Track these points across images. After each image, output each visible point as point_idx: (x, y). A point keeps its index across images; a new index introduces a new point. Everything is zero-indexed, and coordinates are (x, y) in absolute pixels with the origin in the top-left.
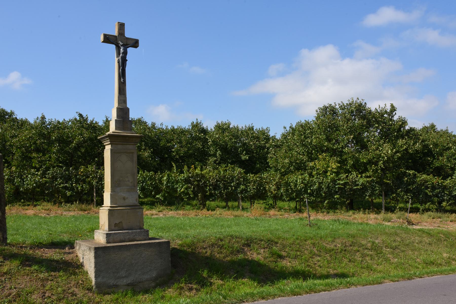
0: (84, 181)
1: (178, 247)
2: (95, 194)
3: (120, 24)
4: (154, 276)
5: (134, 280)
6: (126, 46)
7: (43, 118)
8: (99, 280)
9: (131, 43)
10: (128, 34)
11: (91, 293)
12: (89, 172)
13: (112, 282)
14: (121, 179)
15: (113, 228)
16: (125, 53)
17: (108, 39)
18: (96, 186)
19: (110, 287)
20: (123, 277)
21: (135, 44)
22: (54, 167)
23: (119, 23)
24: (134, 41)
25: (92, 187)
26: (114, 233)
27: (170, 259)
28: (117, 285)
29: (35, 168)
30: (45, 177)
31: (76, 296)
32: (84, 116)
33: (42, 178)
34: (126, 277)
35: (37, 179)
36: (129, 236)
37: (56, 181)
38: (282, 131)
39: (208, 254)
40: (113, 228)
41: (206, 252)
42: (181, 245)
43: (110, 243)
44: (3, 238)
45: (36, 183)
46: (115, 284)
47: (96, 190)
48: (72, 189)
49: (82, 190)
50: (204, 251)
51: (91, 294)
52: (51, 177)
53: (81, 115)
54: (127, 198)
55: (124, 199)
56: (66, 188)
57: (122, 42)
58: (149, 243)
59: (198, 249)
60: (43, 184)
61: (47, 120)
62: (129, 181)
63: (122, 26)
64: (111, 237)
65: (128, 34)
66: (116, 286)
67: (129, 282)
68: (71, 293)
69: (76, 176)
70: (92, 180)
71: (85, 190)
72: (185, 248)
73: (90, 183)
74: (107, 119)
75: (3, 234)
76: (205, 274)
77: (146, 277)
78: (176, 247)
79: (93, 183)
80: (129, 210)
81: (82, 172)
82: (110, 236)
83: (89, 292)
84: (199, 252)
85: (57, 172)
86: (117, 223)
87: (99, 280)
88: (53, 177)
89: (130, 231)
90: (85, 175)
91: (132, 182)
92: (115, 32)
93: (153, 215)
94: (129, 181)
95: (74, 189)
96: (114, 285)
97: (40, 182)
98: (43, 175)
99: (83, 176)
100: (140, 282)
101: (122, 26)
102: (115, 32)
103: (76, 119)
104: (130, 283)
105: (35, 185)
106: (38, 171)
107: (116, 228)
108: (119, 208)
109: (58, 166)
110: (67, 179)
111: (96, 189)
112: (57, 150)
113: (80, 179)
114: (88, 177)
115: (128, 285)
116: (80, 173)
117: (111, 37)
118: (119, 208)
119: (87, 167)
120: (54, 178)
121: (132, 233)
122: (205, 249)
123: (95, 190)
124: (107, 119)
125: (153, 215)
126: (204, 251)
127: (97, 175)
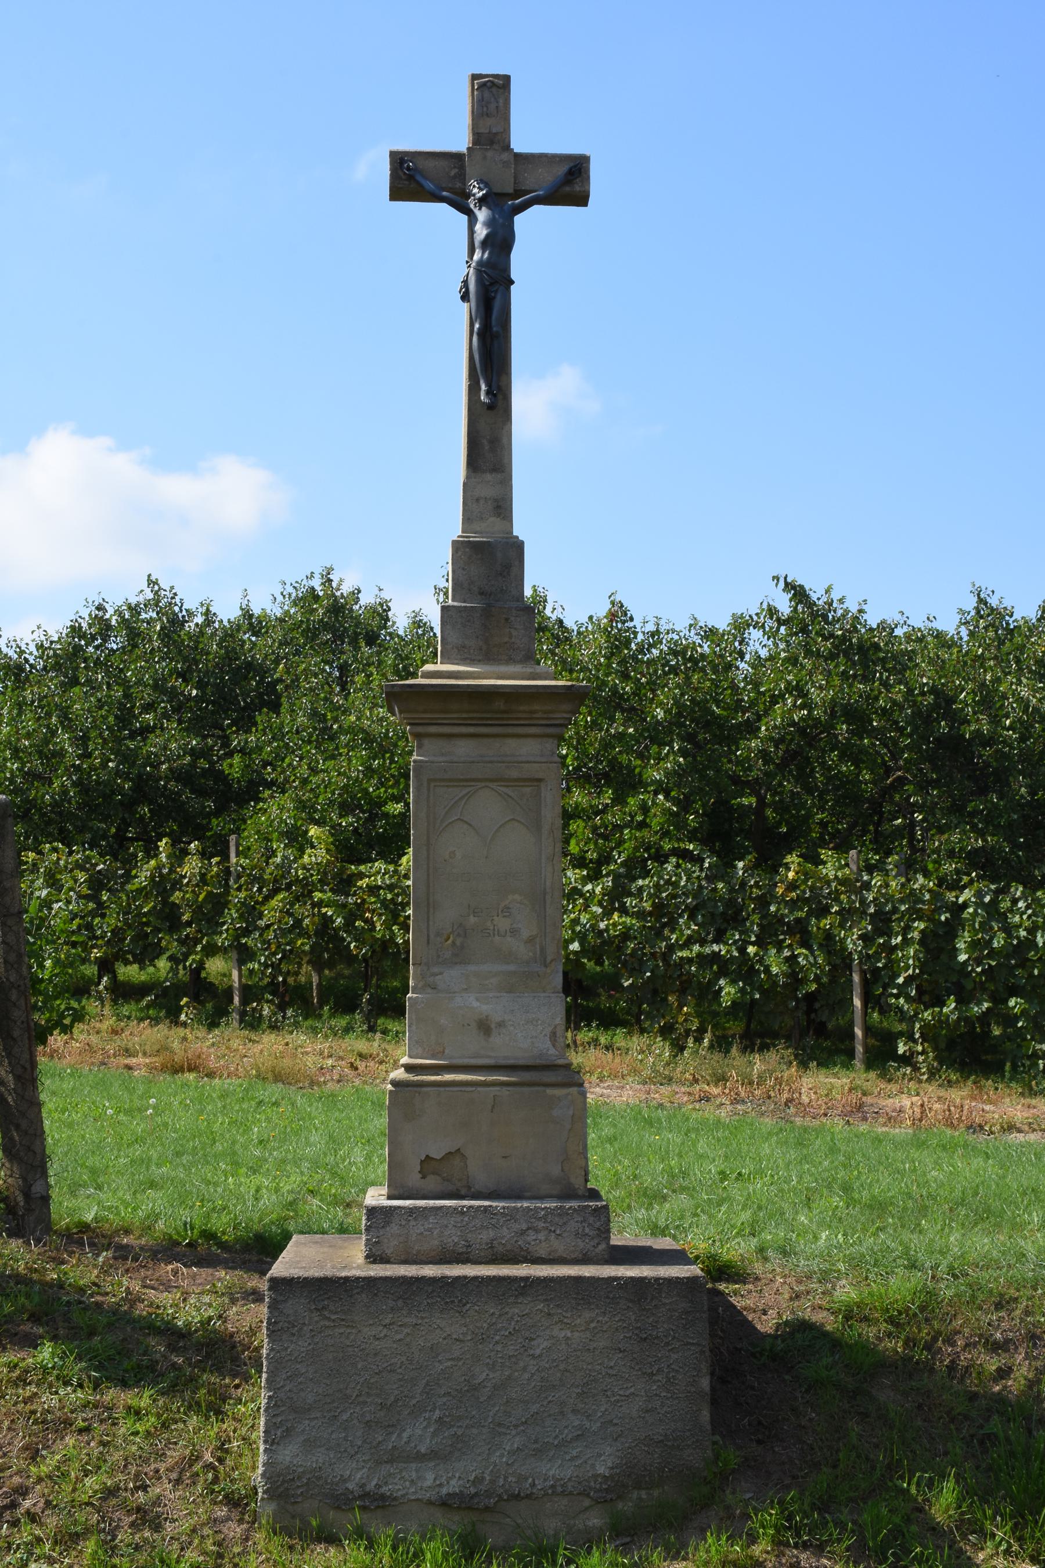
0: (801, 932)
1: (830, 1323)
2: (857, 1002)
3: (482, 86)
4: (601, 1470)
5: (478, 1480)
6: (506, 204)
7: (618, 613)
8: (288, 1454)
9: (545, 179)
10: (530, 134)
11: (241, 1521)
12: (828, 883)
13: (356, 1475)
14: (472, 919)
15: (414, 1179)
16: (500, 242)
17: (413, 178)
18: (866, 958)
19: (342, 1501)
20: (420, 1458)
21: (568, 182)
22: (661, 858)
23: (474, 77)
24: (562, 170)
25: (840, 961)
26: (411, 1211)
27: (705, 1383)
28: (383, 1497)
29: (580, 862)
30: (624, 911)
31: (157, 1528)
32: (817, 594)
33: (607, 914)
34: (433, 1455)
35: (584, 918)
36: (492, 1233)
37: (673, 931)
38: (891, 616)
39: (1015, 1384)
40: (414, 1179)
41: (1003, 1373)
42: (849, 1314)
43: (384, 1260)
44: (27, 1195)
45: (582, 938)
46: (371, 1486)
47: (866, 984)
48: (744, 970)
49: (795, 975)
50: (992, 1364)
51: (234, 1530)
52: (647, 906)
53: (799, 593)
54: (501, 1024)
55: (485, 1027)
56: (722, 966)
57: (491, 180)
58: (579, 1279)
59: (950, 1341)
60: (609, 942)
61: (637, 623)
62: (514, 932)
63: (491, 94)
64: (394, 1228)
65: (530, 134)
66: (378, 1503)
67: (454, 1486)
68: (139, 1509)
69: (763, 903)
70: (842, 926)
71: (804, 981)
72: (870, 1333)
73: (829, 942)
74: (981, 601)
75: (24, 1179)
76: (944, 1503)
77: (554, 1470)
78: (818, 1317)
79: (843, 941)
80: (505, 1091)
81: (792, 886)
82: (387, 1223)
83: (235, 1515)
84: (952, 1367)
85: (675, 885)
86: (438, 1156)
87: (288, 1454)
88: (659, 909)
89: (499, 1204)
90: (807, 901)
91: (531, 940)
92: (453, 134)
93: (1010, 1127)
94: (514, 932)
95: (752, 972)
96: (366, 1495)
97: (601, 932)
98: (614, 900)
99: (794, 905)
100: (517, 1497)
101: (491, 94)
102: (453, 134)
103: (772, 611)
104: (460, 1495)
105: (575, 946)
106: (595, 876)
107: (432, 1183)
108: (449, 1077)
109: (684, 855)
110: (724, 919)
111: (863, 973)
112: (668, 774)
113: (780, 920)
114: (824, 911)
115: (445, 1504)
116: (780, 890)
117: (430, 164)
118: (449, 1077)
119: (818, 862)
120: (663, 915)
121: (510, 1215)
122: (995, 1347)
123: (856, 978)
124: (981, 601)
125: (1010, 1127)
126: (992, 1364)
127: (863, 901)
